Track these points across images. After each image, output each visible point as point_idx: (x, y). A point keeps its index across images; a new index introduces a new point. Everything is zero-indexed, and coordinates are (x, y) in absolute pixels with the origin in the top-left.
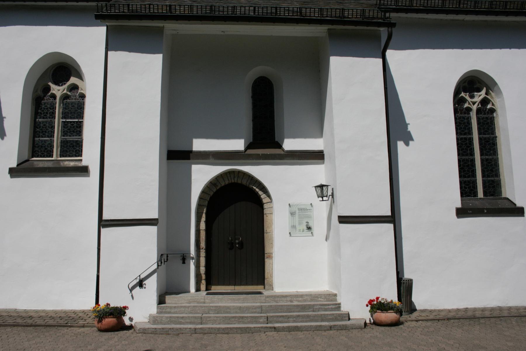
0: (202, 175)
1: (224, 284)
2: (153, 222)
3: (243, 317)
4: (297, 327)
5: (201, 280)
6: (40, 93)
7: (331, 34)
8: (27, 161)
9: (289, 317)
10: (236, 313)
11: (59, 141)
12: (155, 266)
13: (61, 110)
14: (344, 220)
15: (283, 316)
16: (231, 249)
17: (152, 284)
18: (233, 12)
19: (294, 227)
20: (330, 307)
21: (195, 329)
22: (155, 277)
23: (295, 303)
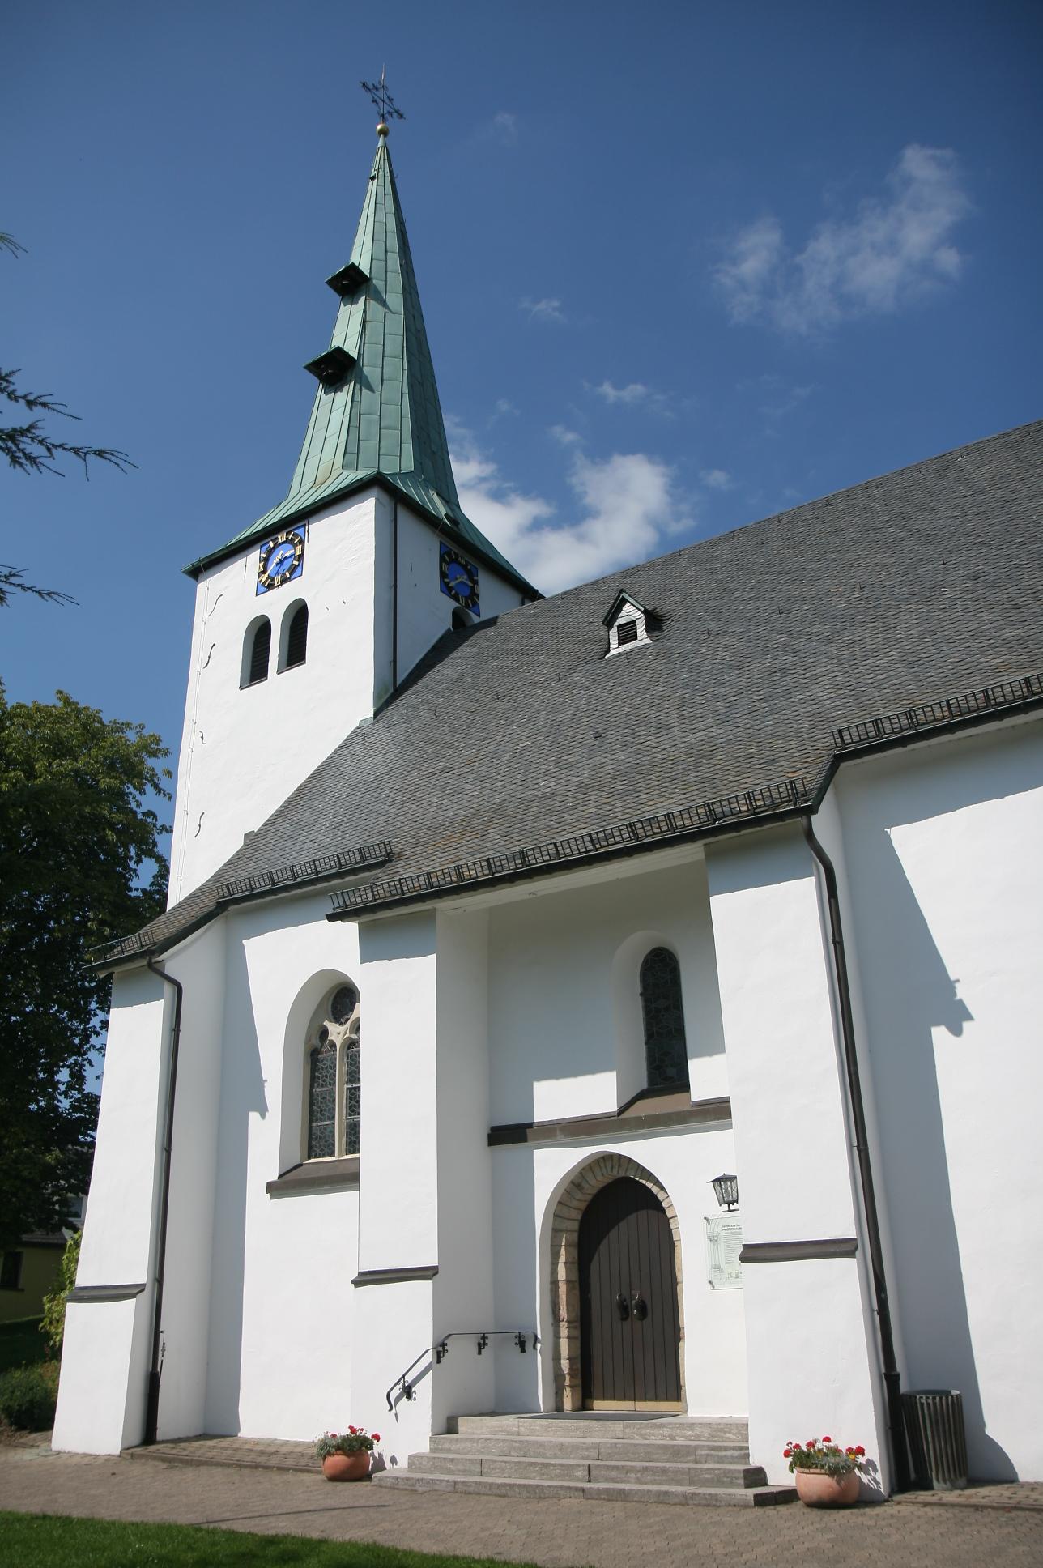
0: (552, 1168)
1: (613, 1397)
2: (430, 1273)
3: (547, 1465)
4: (622, 1491)
5: (564, 1387)
6: (316, 1042)
7: (712, 855)
8: (300, 1165)
9: (628, 1470)
10: (555, 1456)
11: (344, 1125)
12: (429, 1358)
13: (345, 1069)
14: (753, 1253)
15: (617, 1467)
16: (624, 1319)
17: (424, 1390)
18: (987, 700)
19: (717, 1268)
20: (729, 1453)
21: (455, 1483)
22: (428, 1378)
23: (680, 1441)
